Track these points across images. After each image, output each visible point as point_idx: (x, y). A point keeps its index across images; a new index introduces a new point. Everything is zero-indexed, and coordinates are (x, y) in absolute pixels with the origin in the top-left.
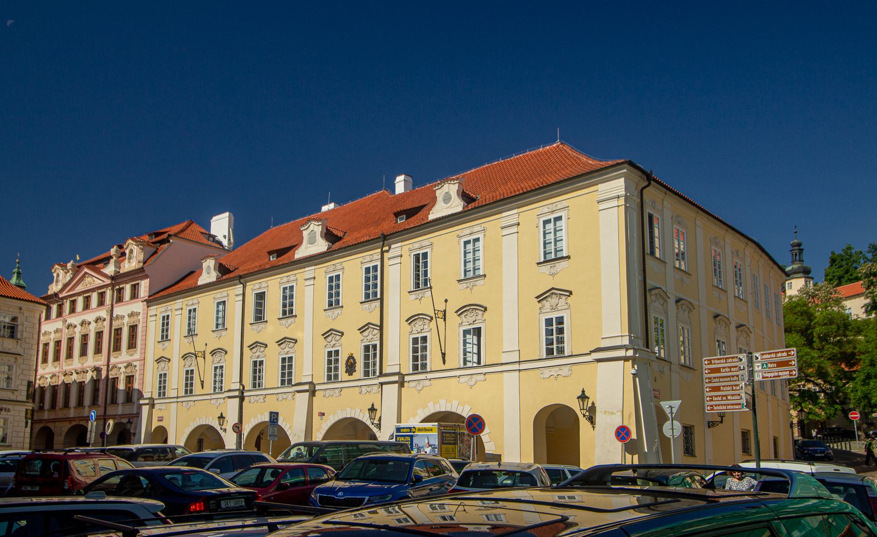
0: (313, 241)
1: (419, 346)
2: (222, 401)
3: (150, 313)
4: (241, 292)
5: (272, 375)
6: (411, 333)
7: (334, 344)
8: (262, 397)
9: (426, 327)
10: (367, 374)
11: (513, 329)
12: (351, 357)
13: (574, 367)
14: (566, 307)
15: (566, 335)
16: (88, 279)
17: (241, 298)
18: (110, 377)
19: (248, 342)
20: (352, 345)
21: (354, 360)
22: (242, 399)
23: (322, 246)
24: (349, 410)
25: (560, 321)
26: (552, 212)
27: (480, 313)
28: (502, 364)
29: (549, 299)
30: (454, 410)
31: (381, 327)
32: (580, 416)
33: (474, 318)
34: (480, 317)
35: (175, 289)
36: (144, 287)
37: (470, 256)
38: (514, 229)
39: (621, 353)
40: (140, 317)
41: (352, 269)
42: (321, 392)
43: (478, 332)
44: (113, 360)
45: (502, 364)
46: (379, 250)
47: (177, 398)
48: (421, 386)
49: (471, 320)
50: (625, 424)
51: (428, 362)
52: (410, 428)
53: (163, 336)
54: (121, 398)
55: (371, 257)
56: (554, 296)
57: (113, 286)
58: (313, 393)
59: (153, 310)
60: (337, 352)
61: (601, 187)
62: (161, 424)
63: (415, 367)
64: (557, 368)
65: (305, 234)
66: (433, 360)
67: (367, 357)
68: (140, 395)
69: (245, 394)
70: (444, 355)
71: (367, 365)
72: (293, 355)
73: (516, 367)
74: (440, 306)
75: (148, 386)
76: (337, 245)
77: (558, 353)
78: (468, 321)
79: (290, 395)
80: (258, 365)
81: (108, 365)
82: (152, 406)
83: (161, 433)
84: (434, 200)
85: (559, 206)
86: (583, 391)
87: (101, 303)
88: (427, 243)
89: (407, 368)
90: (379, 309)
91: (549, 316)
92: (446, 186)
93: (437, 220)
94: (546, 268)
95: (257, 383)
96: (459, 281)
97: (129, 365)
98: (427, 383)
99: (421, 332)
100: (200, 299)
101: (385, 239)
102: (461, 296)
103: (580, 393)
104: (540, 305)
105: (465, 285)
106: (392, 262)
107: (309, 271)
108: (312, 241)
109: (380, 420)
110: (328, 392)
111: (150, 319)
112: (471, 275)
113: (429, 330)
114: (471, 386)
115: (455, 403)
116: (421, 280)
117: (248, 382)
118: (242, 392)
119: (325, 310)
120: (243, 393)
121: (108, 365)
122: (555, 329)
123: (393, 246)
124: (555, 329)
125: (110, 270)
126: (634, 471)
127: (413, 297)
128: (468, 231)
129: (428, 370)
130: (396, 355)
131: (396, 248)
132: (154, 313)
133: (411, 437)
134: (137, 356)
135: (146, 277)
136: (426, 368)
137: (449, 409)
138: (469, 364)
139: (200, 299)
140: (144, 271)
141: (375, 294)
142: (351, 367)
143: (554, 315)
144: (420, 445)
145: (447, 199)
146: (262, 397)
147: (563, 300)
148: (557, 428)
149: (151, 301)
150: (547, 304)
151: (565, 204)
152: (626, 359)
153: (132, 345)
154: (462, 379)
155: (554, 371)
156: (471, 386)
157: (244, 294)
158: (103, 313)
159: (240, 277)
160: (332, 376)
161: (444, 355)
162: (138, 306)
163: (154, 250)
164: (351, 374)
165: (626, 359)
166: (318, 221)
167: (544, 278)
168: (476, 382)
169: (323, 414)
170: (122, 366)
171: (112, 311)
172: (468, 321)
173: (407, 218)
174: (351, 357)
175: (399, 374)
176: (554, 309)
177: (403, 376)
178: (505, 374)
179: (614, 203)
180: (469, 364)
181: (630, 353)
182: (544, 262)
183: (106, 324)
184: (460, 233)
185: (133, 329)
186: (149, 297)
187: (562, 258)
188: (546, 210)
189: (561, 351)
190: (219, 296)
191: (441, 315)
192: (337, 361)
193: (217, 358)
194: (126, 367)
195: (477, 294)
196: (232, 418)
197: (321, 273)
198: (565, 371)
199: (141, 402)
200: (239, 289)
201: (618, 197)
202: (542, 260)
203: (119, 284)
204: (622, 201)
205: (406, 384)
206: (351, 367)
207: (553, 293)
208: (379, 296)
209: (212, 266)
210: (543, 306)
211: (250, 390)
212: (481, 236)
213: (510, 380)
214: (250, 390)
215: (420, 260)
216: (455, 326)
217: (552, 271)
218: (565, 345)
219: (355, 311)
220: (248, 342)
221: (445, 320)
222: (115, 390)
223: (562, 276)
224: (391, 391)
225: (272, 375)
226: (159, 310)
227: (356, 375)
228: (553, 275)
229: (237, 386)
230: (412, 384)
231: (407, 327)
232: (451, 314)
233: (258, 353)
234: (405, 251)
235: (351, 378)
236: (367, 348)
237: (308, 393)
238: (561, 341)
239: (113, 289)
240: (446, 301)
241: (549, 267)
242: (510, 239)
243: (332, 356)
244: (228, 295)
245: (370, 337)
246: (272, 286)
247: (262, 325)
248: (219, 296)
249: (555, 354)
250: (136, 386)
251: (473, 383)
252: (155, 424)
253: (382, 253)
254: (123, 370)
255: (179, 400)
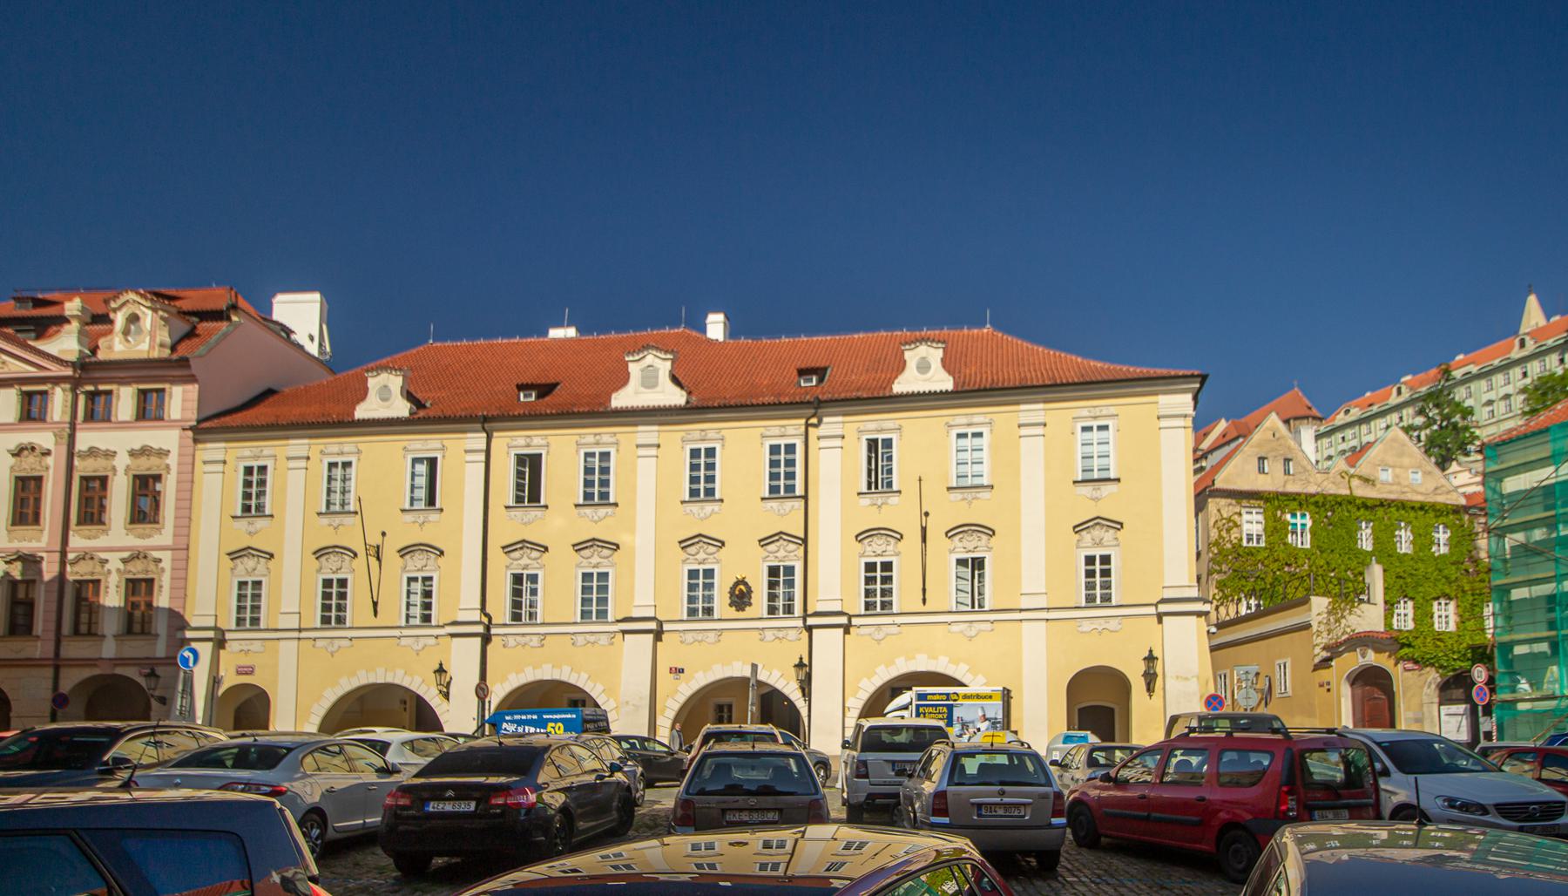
0: (649, 380)
1: (878, 576)
2: (432, 641)
4: (484, 447)
6: (319, 570)
7: (701, 558)
9: (890, 548)
10: (772, 610)
11: (1034, 562)
13: (1125, 620)
15: (263, 603)
17: (482, 457)
18: (71, 578)
22: (486, 639)
23: (402, 409)
24: (566, 669)
25: (1106, 560)
26: (1095, 418)
27: (984, 537)
28: (1021, 610)
33: (975, 543)
34: (431, 562)
35: (237, 419)
36: (181, 400)
37: (337, 485)
41: (743, 447)
43: (978, 564)
44: (77, 541)
45: (1021, 610)
46: (803, 421)
47: (300, 630)
51: (348, 614)
54: (110, 626)
55: (789, 429)
57: (75, 383)
58: (658, 635)
59: (213, 450)
60: (709, 573)
61: (1162, 399)
65: (634, 369)
68: (177, 621)
69: (493, 631)
70: (375, 604)
71: (772, 597)
74: (374, 539)
75: (206, 601)
76: (422, 414)
78: (966, 547)
81: (64, 553)
82: (220, 643)
83: (249, 706)
84: (901, 366)
91: (1090, 553)
94: (1086, 490)
96: (949, 489)
98: (894, 629)
99: (421, 570)
100: (361, 446)
101: (815, 407)
107: (647, 433)
108: (650, 381)
113: (356, 573)
114: (879, 641)
115: (381, 671)
116: (878, 476)
117: (500, 608)
119: (319, 514)
120: (488, 628)
121: (64, 553)
122: (1098, 569)
123: (825, 420)
124: (1098, 569)
125: (66, 344)
127: (866, 501)
128: (964, 420)
131: (832, 424)
132: (221, 457)
133: (950, 708)
134: (163, 536)
135: (191, 379)
138: (412, 622)
139: (361, 446)
140: (189, 367)
141: (790, 489)
144: (966, 719)
145: (649, 380)
146: (535, 638)
148: (1097, 703)
149: (206, 427)
151: (1113, 410)
152: (1199, 614)
154: (954, 628)
159: (486, 419)
160: (699, 609)
161: (375, 604)
163: (185, 328)
165: (1199, 614)
166: (666, 352)
167: (1085, 504)
169: (682, 671)
172: (966, 547)
173: (538, 397)
175: (215, 629)
176: (1099, 544)
178: (1024, 624)
179: (1180, 422)
180: (412, 622)
186: (199, 422)
187: (1108, 480)
188: (1085, 413)
190: (418, 445)
191: (372, 552)
197: (677, 441)
198: (1113, 624)
200: (477, 440)
203: (95, 382)
204: (1189, 422)
205: (664, 637)
208: (799, 491)
212: (353, 459)
216: (395, 572)
217: (251, 529)
218: (1113, 590)
219: (744, 516)
221: (378, 559)
222: (94, 609)
227: (749, 612)
228: (1096, 499)
229: (476, 616)
230: (863, 630)
232: (390, 554)
233: (525, 561)
235: (741, 615)
236: (773, 571)
238: (256, 608)
239: (74, 390)
240: (384, 534)
243: (700, 580)
246: (563, 451)
247: (534, 513)
248: (418, 445)
250: (162, 600)
252: (229, 679)
253: (807, 425)
255: (303, 634)
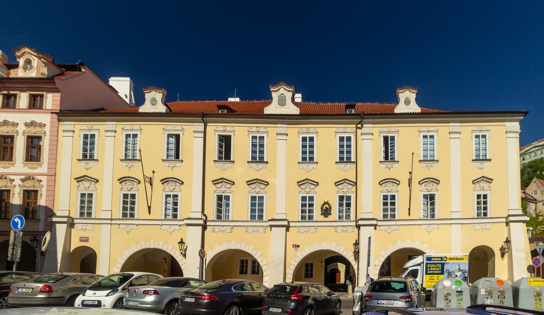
1: (389, 202)
3: (61, 128)
4: (203, 130)
5: (239, 207)
7: (308, 190)
11: (456, 198)
14: (489, 189)
17: (202, 135)
20: (326, 194)
22: (204, 227)
26: (481, 131)
28: (100, 219)
30: (160, 248)
42: (211, 227)
45: (100, 219)
47: (112, 220)
52: (442, 258)
60: (311, 198)
61: (508, 124)
65: (275, 95)
67: (341, 205)
68: (50, 212)
69: (208, 224)
70: (149, 208)
72: (314, 195)
74: (149, 174)
77: (484, 215)
80: (222, 201)
82: (71, 225)
85: (484, 129)
86: (182, 239)
89: (76, 214)
91: (479, 193)
92: (153, 92)
93: (400, 114)
94: (478, 164)
97: (28, 178)
98: (396, 227)
102: (421, 171)
104: (473, 186)
105: (424, 165)
106: (364, 137)
109: (186, 249)
113: (139, 191)
115: (162, 243)
116: (389, 155)
117: (211, 212)
119: (299, 163)
122: (482, 201)
123: (364, 125)
124: (482, 201)
126: (24, 285)
127: (383, 165)
131: (368, 128)
133: (443, 265)
137: (156, 247)
138: (168, 217)
142: (326, 211)
143: (482, 193)
144: (451, 270)
146: (228, 228)
149: (64, 114)
151: (488, 128)
156: (429, 232)
161: (149, 208)
162: (44, 118)
169: (298, 246)
176: (483, 189)
177: (73, 219)
178: (103, 225)
182: (125, 160)
189: (89, 214)
190: (170, 128)
191: (148, 180)
192: (311, 205)
195: (433, 171)
197: (295, 133)
199: (54, 219)
202: (124, 158)
206: (326, 211)
211: (213, 221)
213: (456, 230)
214: (213, 221)
215: (89, 141)
217: (87, 166)
219: (327, 168)
221: (151, 184)
223: (487, 170)
225: (239, 207)
227: (330, 218)
231: (118, 185)
232: (157, 182)
235: (326, 219)
237: (65, 225)
238: (90, 208)
242: (455, 140)
244: (141, 130)
248: (170, 128)
249: (86, 216)
250: (42, 202)
252: (75, 244)
255: (113, 222)
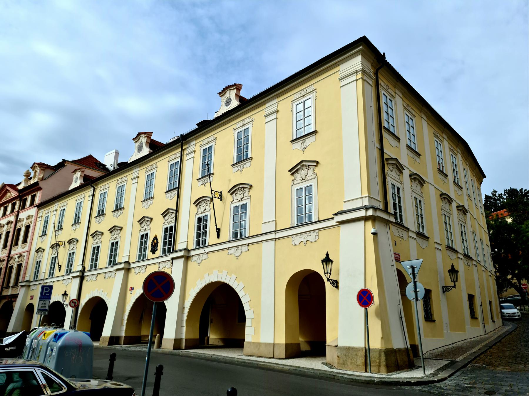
1: (202, 224)
3: (39, 215)
4: (92, 193)
8: (95, 276)
9: (207, 207)
12: (156, 238)
14: (314, 176)
16: (9, 194)
19: (91, 232)
21: (157, 241)
26: (303, 96)
27: (247, 190)
29: (300, 172)
31: (177, 211)
32: (325, 280)
38: (274, 116)
39: (362, 213)
40: (33, 219)
46: (180, 150)
48: (240, 251)
49: (239, 197)
50: (368, 287)
53: (140, 255)
56: (304, 168)
60: (147, 235)
62: (31, 301)
63: (198, 243)
64: (306, 235)
66: (211, 237)
69: (86, 274)
73: (272, 236)
78: (237, 199)
79: (113, 273)
80: (96, 249)
85: (309, 91)
86: (327, 255)
87: (12, 211)
88: (212, 138)
90: (176, 197)
95: (94, 266)
98: (205, 256)
103: (324, 257)
104: (292, 178)
110: (107, 274)
111: (38, 219)
112: (242, 158)
118: (83, 271)
120: (83, 273)
129: (207, 244)
130: (185, 237)
136: (205, 244)
140: (38, 184)
147: (310, 172)
150: (298, 176)
151: (313, 87)
152: (366, 219)
153: (25, 241)
154: (232, 251)
155: (303, 238)
157: (93, 195)
158: (12, 218)
164: (154, 253)
165: (366, 219)
168: (241, 253)
170: (16, 257)
171: (17, 216)
174: (156, 238)
176: (303, 180)
178: (264, 244)
179: (354, 78)
181: (370, 212)
183: (13, 225)
184: (235, 127)
185: (28, 227)
191: (217, 195)
193: (72, 246)
194: (19, 257)
196: (73, 295)
198: (312, 237)
201: (357, 72)
204: (360, 75)
207: (303, 166)
209: (79, 177)
210: (295, 178)
216: (230, 202)
220: (91, 232)
224: (179, 264)
226: (43, 212)
234: (197, 148)
241: (300, 143)
245: (170, 220)
251: (199, 262)
254: (17, 260)
